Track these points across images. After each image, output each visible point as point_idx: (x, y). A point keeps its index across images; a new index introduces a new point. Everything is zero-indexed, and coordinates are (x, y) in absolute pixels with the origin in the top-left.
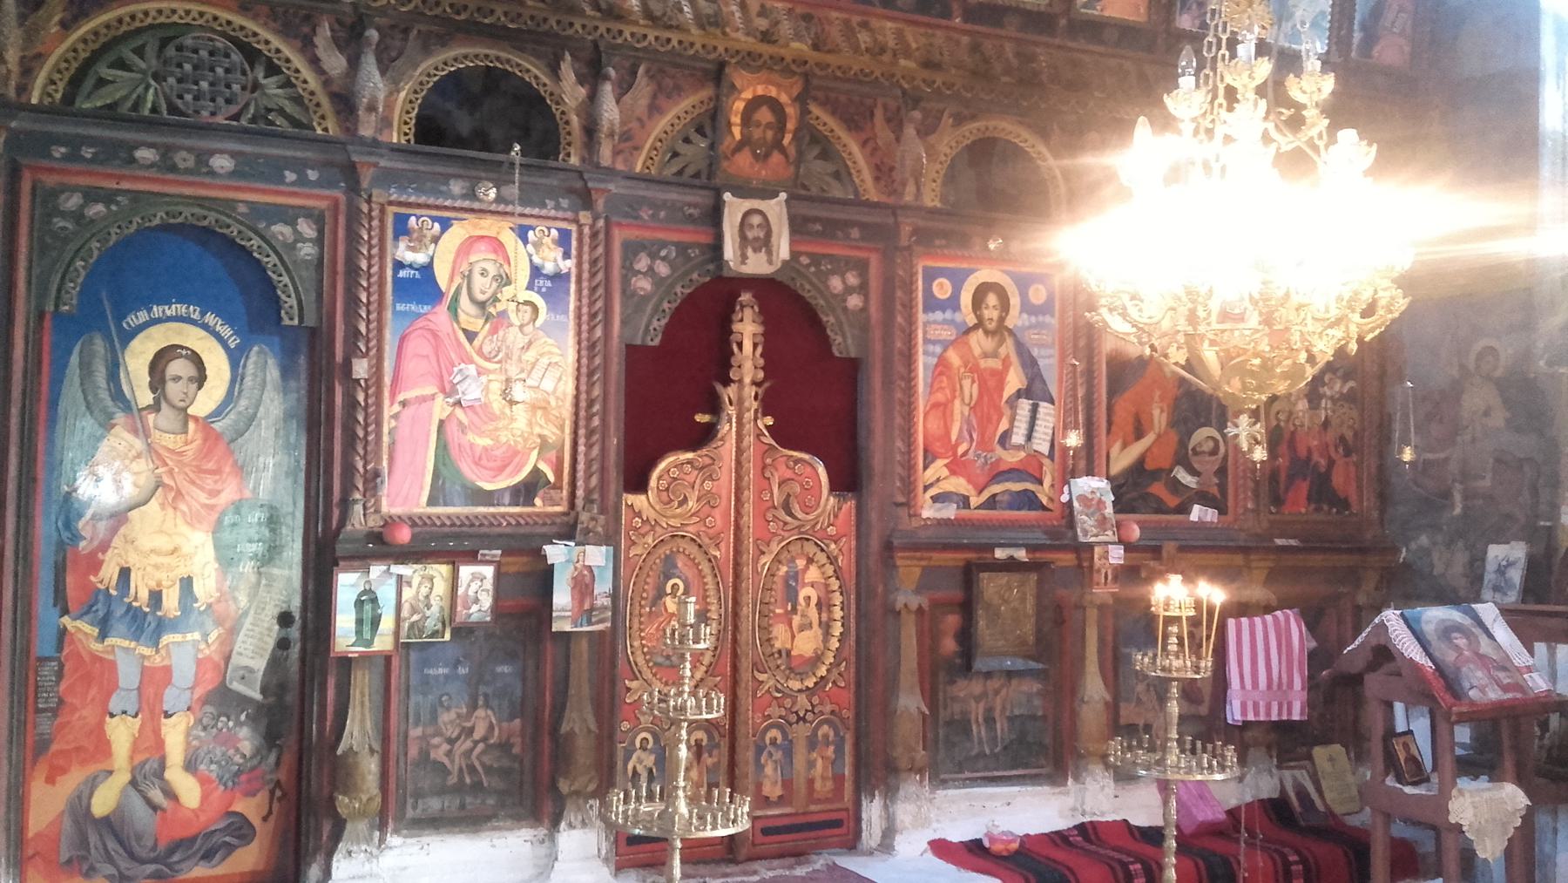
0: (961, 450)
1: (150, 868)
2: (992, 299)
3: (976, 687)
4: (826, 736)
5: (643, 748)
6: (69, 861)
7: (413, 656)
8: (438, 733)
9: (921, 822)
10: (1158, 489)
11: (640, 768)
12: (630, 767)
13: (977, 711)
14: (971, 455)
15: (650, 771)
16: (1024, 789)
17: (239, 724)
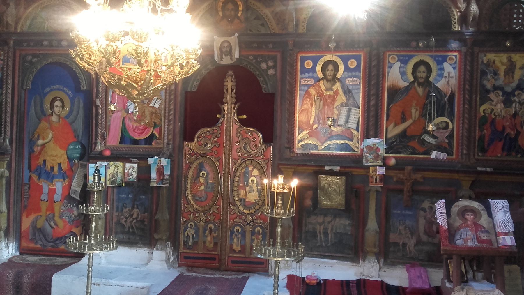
0: (314, 127)
1: (51, 244)
2: (330, 67)
3: (320, 219)
4: (259, 231)
5: (191, 227)
6: (31, 239)
7: (115, 190)
8: (122, 215)
9: (287, 267)
10: (414, 144)
11: (189, 234)
12: (186, 233)
13: (320, 229)
14: (319, 129)
15: (193, 235)
16: (338, 262)
17: (73, 206)
